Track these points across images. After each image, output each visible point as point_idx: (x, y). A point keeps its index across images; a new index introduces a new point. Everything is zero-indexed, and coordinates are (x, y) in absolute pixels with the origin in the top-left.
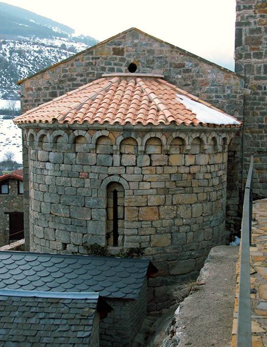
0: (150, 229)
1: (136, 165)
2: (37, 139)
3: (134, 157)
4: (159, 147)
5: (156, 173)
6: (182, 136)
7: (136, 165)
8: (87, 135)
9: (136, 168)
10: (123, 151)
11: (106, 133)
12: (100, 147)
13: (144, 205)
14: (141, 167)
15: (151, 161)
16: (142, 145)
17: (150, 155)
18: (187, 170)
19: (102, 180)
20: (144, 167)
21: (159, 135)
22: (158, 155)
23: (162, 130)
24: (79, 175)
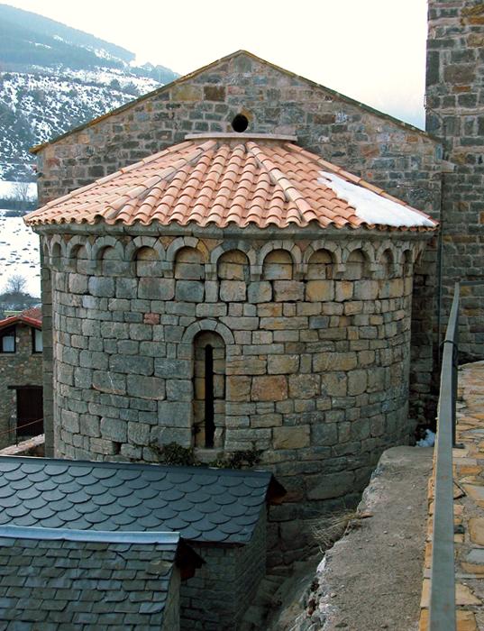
0: (272, 416)
1: (247, 301)
2: (66, 253)
3: (243, 286)
4: (289, 267)
5: (283, 315)
6: (330, 246)
7: (247, 301)
8: (158, 246)
9: (246, 305)
10: (222, 275)
11: (192, 242)
12: (181, 268)
13: (260, 372)
14: (256, 304)
15: (274, 293)
16: (257, 264)
17: (272, 282)
18: (339, 309)
19: (186, 328)
20: (261, 303)
21: (287, 246)
22: (287, 282)
23: (293, 237)
24: (144, 318)
